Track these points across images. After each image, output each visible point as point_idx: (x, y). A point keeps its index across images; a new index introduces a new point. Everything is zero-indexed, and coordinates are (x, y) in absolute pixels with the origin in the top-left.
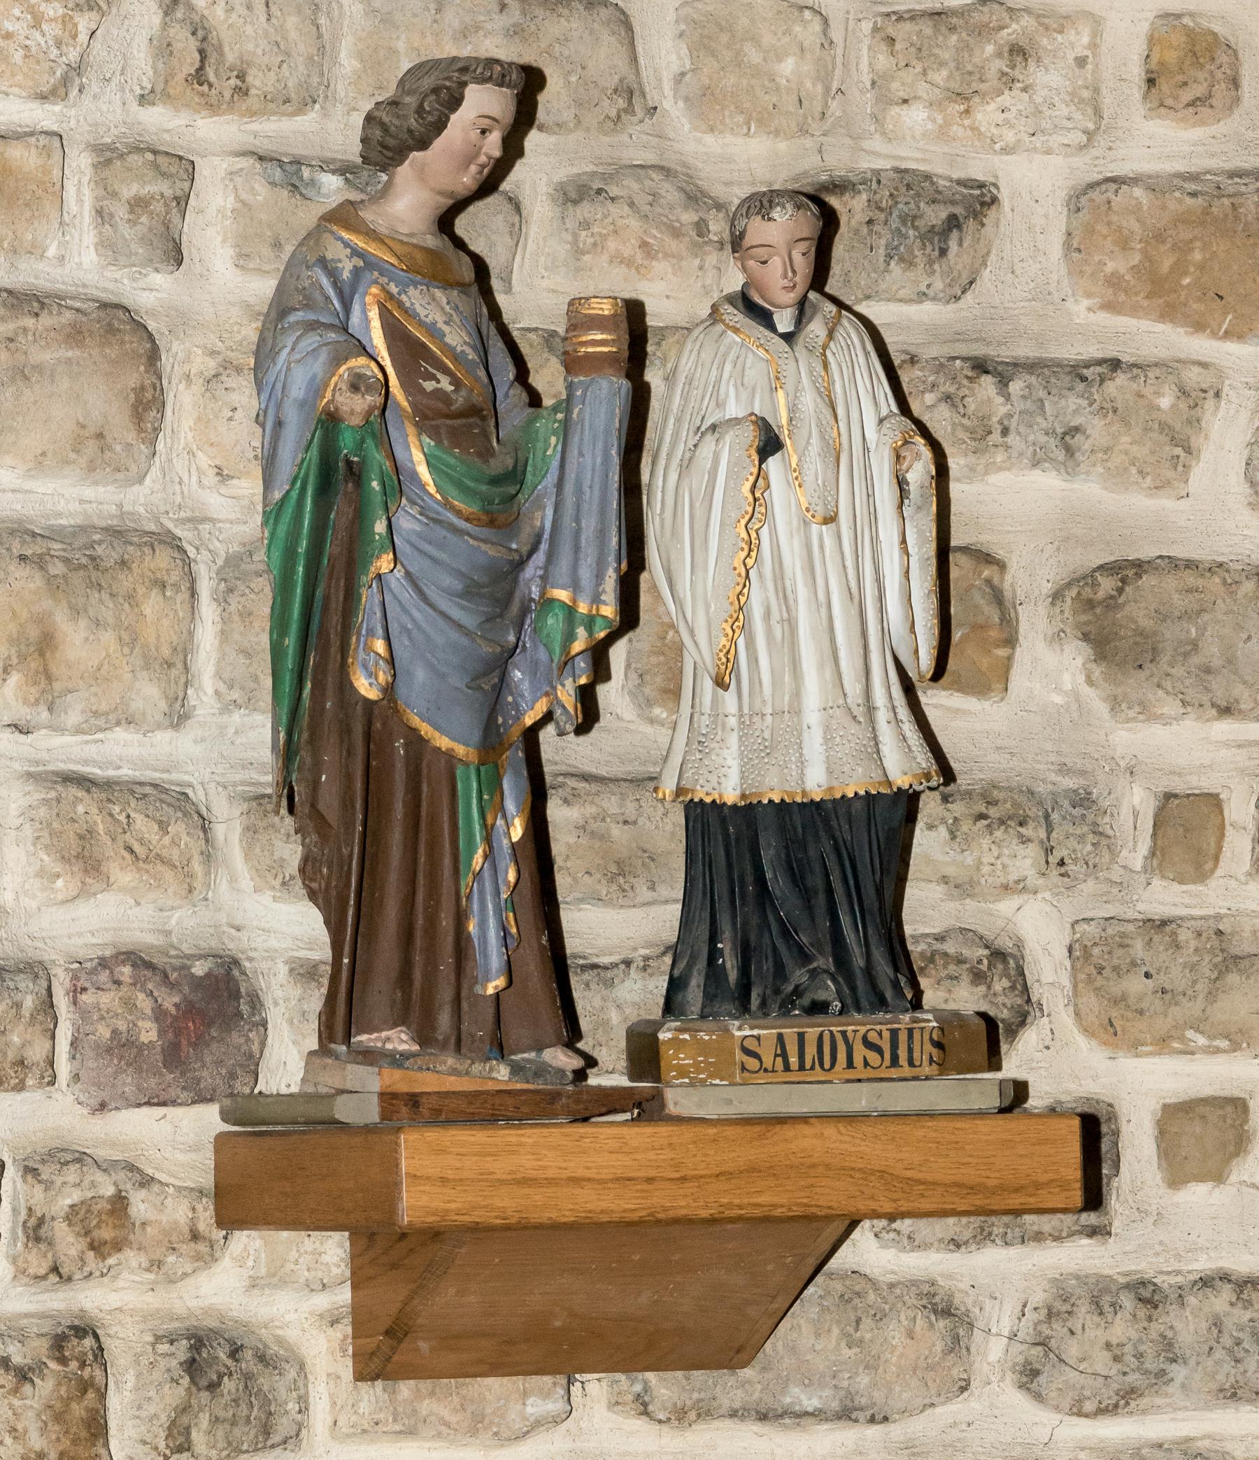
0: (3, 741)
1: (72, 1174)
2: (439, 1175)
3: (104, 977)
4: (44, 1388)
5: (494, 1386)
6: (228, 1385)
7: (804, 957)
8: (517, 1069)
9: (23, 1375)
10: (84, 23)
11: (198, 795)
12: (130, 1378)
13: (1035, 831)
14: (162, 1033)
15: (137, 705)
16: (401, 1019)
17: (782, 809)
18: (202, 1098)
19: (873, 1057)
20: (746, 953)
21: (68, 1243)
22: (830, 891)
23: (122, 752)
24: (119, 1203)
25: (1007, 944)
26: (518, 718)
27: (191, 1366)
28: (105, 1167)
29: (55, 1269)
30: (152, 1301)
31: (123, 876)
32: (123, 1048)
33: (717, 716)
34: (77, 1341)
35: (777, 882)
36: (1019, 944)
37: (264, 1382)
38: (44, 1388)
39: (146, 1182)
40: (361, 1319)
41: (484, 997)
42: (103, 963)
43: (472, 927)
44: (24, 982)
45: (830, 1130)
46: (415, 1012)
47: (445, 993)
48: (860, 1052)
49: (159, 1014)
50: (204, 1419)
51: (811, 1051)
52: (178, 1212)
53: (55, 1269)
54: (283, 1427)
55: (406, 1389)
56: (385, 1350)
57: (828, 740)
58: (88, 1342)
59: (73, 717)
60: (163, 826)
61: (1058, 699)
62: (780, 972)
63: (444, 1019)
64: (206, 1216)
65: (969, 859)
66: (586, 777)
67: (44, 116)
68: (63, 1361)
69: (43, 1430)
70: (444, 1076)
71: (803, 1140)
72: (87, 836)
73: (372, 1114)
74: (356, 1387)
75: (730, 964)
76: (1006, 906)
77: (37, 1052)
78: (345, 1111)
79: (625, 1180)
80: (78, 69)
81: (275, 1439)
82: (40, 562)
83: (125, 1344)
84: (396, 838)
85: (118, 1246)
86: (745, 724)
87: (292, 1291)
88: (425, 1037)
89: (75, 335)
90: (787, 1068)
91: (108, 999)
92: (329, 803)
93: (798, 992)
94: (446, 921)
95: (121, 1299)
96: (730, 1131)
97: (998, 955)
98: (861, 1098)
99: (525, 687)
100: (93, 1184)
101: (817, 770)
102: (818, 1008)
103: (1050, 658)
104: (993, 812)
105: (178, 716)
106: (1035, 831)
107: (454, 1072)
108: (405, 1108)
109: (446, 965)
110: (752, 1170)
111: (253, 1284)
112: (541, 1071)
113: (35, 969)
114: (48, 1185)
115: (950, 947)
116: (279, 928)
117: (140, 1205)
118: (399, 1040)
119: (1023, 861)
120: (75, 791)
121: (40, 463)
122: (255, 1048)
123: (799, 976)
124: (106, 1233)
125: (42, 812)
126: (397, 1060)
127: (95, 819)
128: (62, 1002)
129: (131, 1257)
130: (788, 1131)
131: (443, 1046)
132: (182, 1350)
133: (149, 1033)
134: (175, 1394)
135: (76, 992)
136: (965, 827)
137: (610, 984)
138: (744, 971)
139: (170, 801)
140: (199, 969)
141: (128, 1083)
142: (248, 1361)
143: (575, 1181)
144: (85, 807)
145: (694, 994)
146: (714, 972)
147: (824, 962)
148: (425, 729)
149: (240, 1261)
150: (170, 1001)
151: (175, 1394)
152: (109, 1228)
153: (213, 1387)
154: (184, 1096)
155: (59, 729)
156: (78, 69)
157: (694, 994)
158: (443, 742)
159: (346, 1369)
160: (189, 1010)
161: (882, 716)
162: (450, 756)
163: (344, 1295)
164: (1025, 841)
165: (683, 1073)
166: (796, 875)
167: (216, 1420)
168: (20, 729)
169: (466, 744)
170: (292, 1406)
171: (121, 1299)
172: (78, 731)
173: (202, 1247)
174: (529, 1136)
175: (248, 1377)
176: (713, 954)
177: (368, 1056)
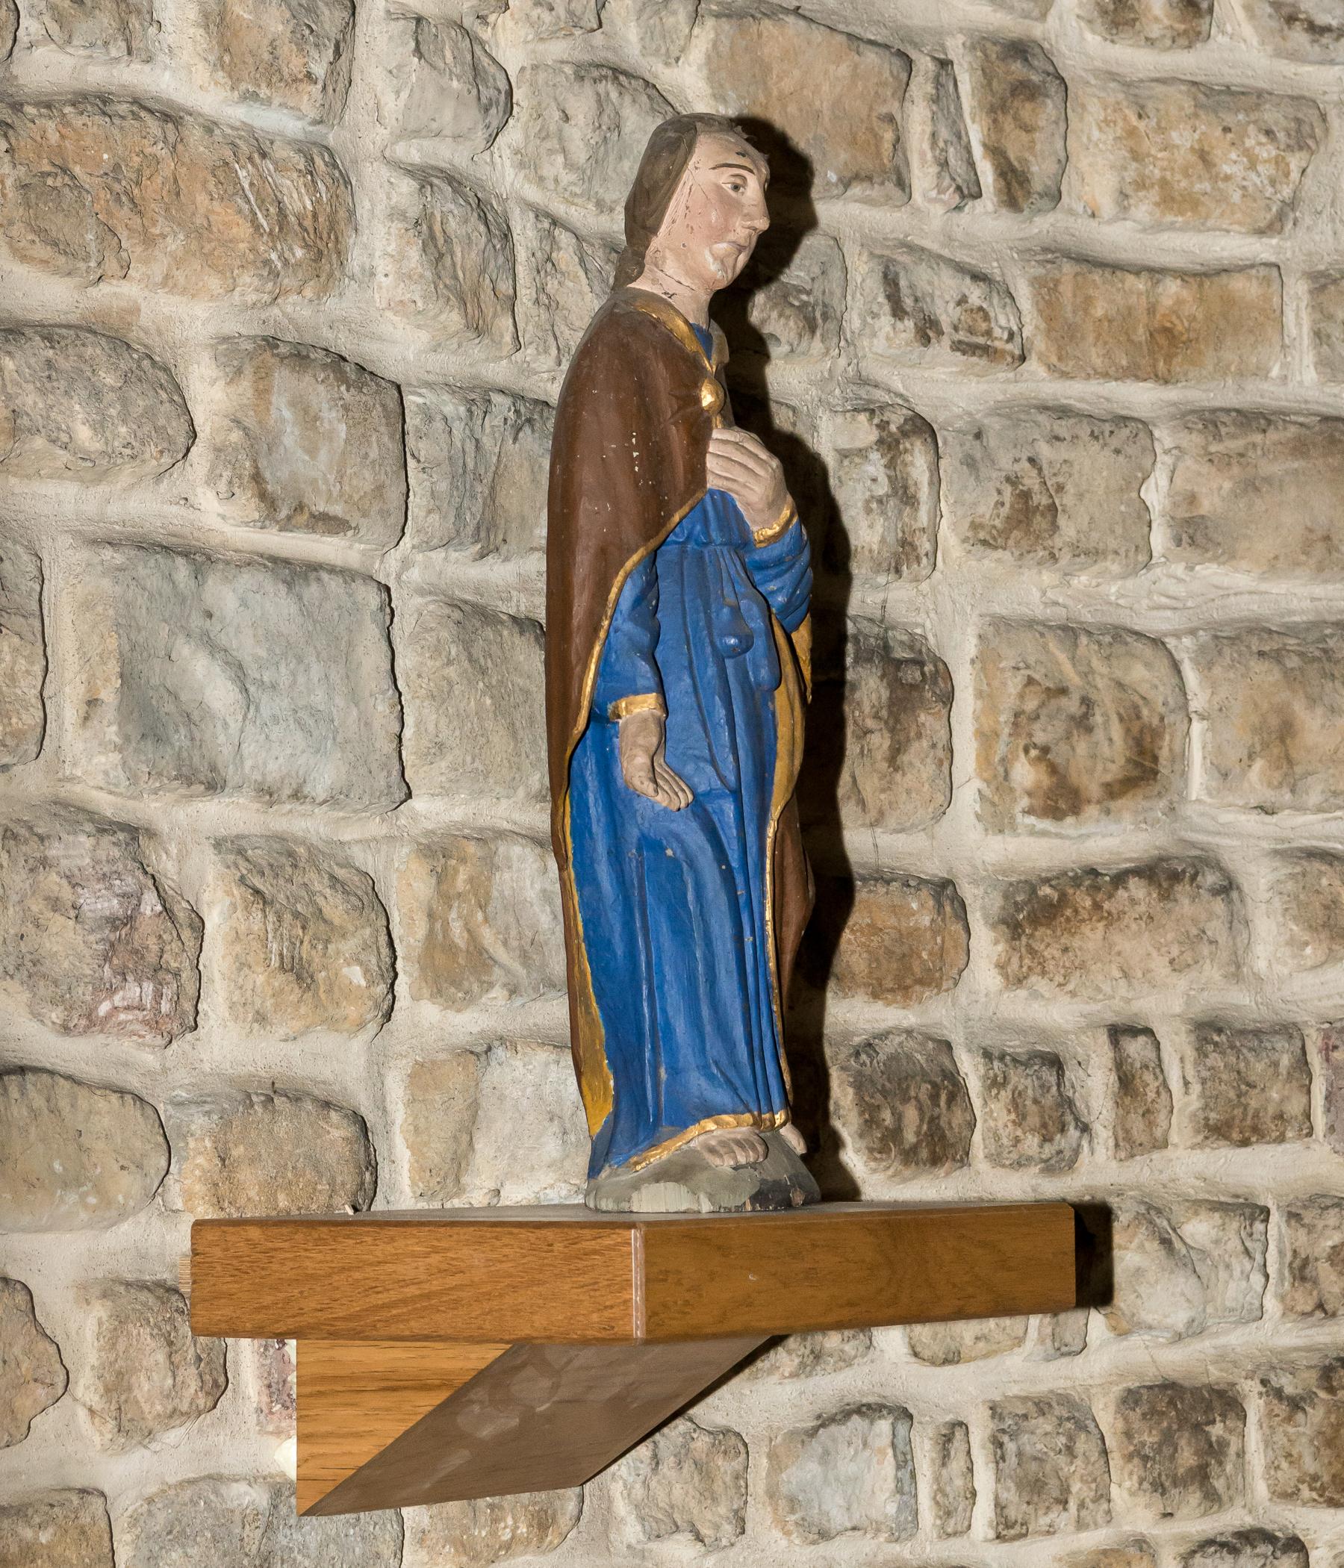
4: (1316, 1416)
9: (1296, 1405)
10: (1295, 161)
38: (1316, 1416)
67: (1263, 249)
80: (1292, 204)
82: (1277, 656)
89: (1300, 448)
113: (1289, 1030)
121: (1273, 567)
156: (1292, 204)
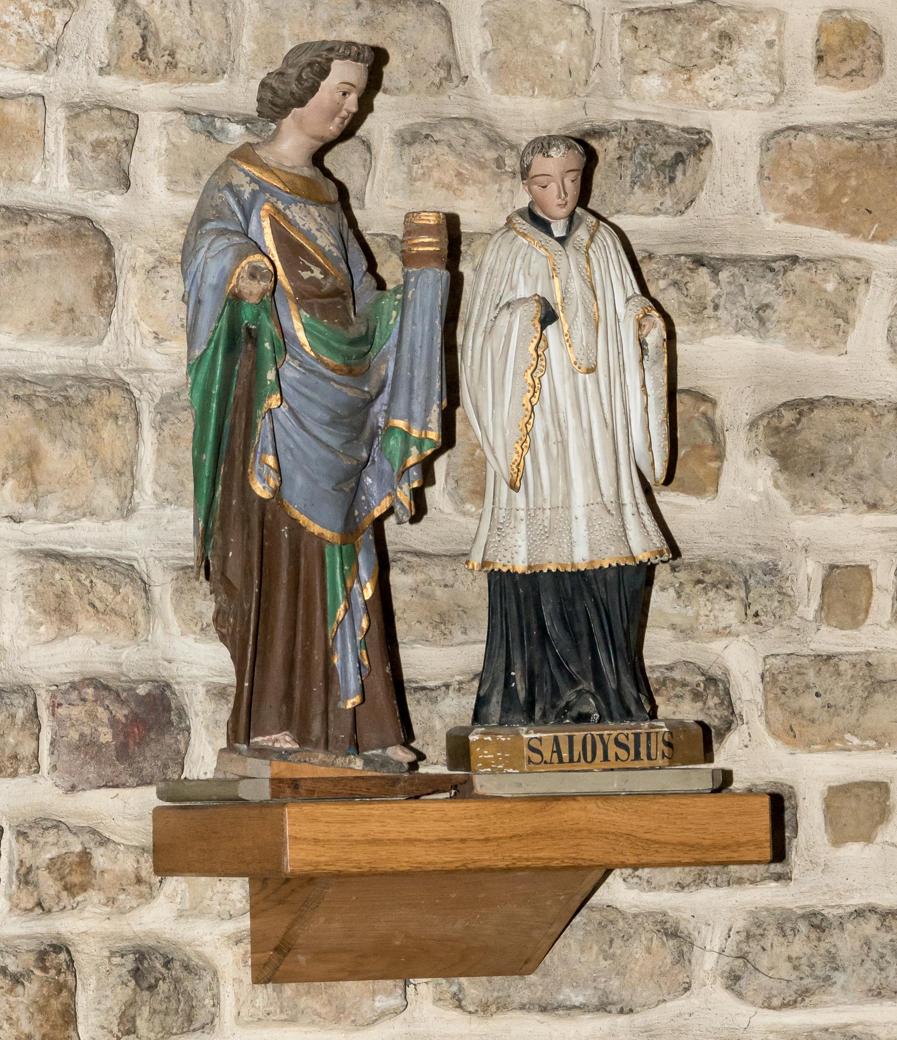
0: (2, 528)
1: (51, 836)
2: (313, 837)
3: (74, 696)
4: (32, 989)
5: (352, 987)
6: (163, 986)
7: (573, 682)
8: (368, 762)
11: (141, 567)
12: (93, 981)
13: (737, 592)
14: (115, 736)
15: (97, 502)
16: (285, 726)
17: (557, 576)
18: (144, 782)
19: (622, 753)
20: (531, 679)
21: (49, 885)
22: (591, 635)
23: (87, 536)
24: (85, 857)
25: (717, 672)
26: (369, 511)
27: (136, 973)
28: (75, 831)
29: (39, 904)
30: (108, 927)
31: (88, 624)
32: (88, 746)
33: (511, 510)
34: (55, 955)
35: (554, 628)
36: (726, 673)
37: (188, 984)
38: (32, 989)
39: (104, 842)
40: (257, 939)
41: (345, 710)
42: (73, 686)
43: (336, 660)
44: (17, 700)
45: (591, 805)
46: (296, 721)
47: (317, 708)
48: (613, 749)
49: (113, 722)
50: (146, 1011)
51: (578, 748)
52: (127, 864)
53: (39, 904)
54: (202, 1016)
55: (289, 989)
56: (274, 962)
57: (590, 527)
58: (63, 956)
59: (52, 511)
60: (116, 589)
61: (754, 498)
62: (556, 692)
63: (317, 726)
64: (147, 866)
65: (691, 612)
66: (417, 554)
68: (45, 969)
69: (31, 1019)
70: (316, 766)
71: (572, 812)
72: (62, 595)
73: (265, 793)
74: (253, 988)
75: (520, 686)
76: (717, 646)
77: (26, 750)
78: (246, 791)
79: (445, 841)
81: (196, 1025)
83: (89, 957)
84: (282, 597)
85: (84, 888)
86: (531, 516)
87: (208, 919)
88: (303, 739)
90: (561, 761)
91: (77, 712)
92: (235, 572)
93: (569, 706)
94: (318, 656)
95: (86, 926)
96: (520, 806)
97: (711, 680)
98: (613, 782)
99: (374, 489)
100: (66, 844)
101: (582, 548)
102: (583, 718)
103: (748, 468)
104: (708, 578)
105: (127, 510)
106: (737, 592)
107: (324, 763)
108: (288, 789)
109: (318, 688)
110: (536, 833)
111: (181, 915)
112: (385, 763)
113: (25, 690)
114: (34, 844)
115: (677, 675)
116: (198, 661)
117: (100, 859)
118: (285, 741)
119: (729, 613)
120: (53, 564)
122: (182, 746)
123: (569, 695)
124: (75, 879)
125: (30, 578)
126: (283, 755)
127: (68, 584)
128: (44, 714)
129: (94, 896)
130: (562, 806)
131: (316, 745)
132: (129, 962)
133: (106, 736)
134: (125, 993)
135: (54, 706)
136: (688, 589)
137: (434, 701)
138: (530, 691)
139: (121, 571)
140: (142, 690)
141: (91, 771)
142: (177, 970)
143: (410, 841)
144: (61, 575)
145: (494, 708)
146: (509, 693)
147: (587, 685)
148: (303, 520)
149: (171, 899)
150: (121, 713)
151: (125, 993)
152: (77, 875)
153: (152, 988)
154: (131, 780)
155: (42, 519)
157: (494, 708)
158: (316, 529)
159: (247, 975)
160: (135, 719)
161: (629, 510)
162: (320, 538)
163: (245, 923)
164: (730, 599)
165: (486, 764)
166: (567, 623)
167: (154, 1012)
168: (15, 519)
169: (332, 530)
170: (208, 1002)
171: (86, 926)
172: (56, 521)
173: (144, 889)
174: (377, 809)
175: (177, 981)
176: (508, 679)
177: (262, 753)
